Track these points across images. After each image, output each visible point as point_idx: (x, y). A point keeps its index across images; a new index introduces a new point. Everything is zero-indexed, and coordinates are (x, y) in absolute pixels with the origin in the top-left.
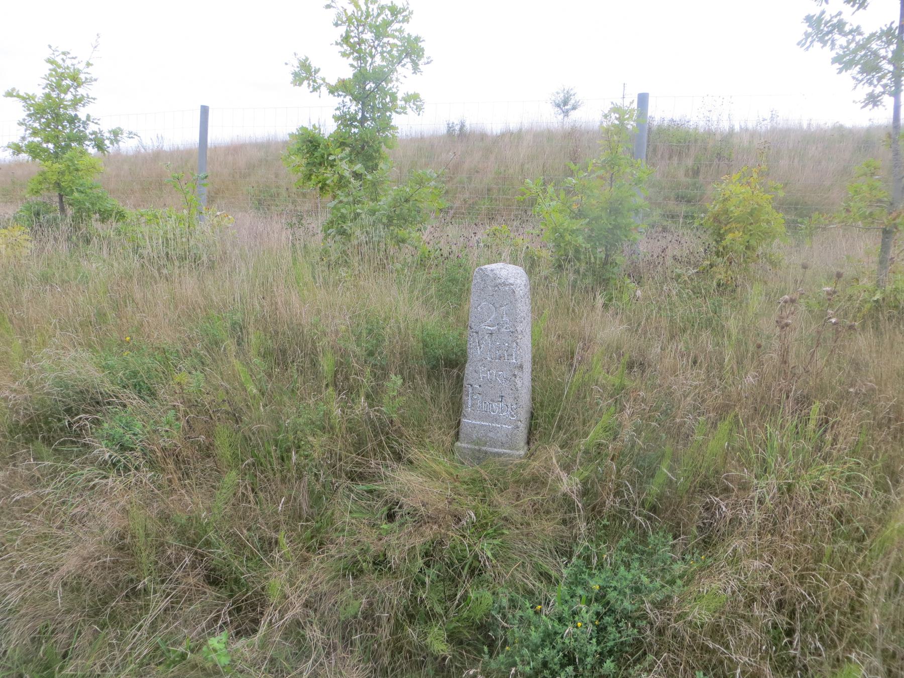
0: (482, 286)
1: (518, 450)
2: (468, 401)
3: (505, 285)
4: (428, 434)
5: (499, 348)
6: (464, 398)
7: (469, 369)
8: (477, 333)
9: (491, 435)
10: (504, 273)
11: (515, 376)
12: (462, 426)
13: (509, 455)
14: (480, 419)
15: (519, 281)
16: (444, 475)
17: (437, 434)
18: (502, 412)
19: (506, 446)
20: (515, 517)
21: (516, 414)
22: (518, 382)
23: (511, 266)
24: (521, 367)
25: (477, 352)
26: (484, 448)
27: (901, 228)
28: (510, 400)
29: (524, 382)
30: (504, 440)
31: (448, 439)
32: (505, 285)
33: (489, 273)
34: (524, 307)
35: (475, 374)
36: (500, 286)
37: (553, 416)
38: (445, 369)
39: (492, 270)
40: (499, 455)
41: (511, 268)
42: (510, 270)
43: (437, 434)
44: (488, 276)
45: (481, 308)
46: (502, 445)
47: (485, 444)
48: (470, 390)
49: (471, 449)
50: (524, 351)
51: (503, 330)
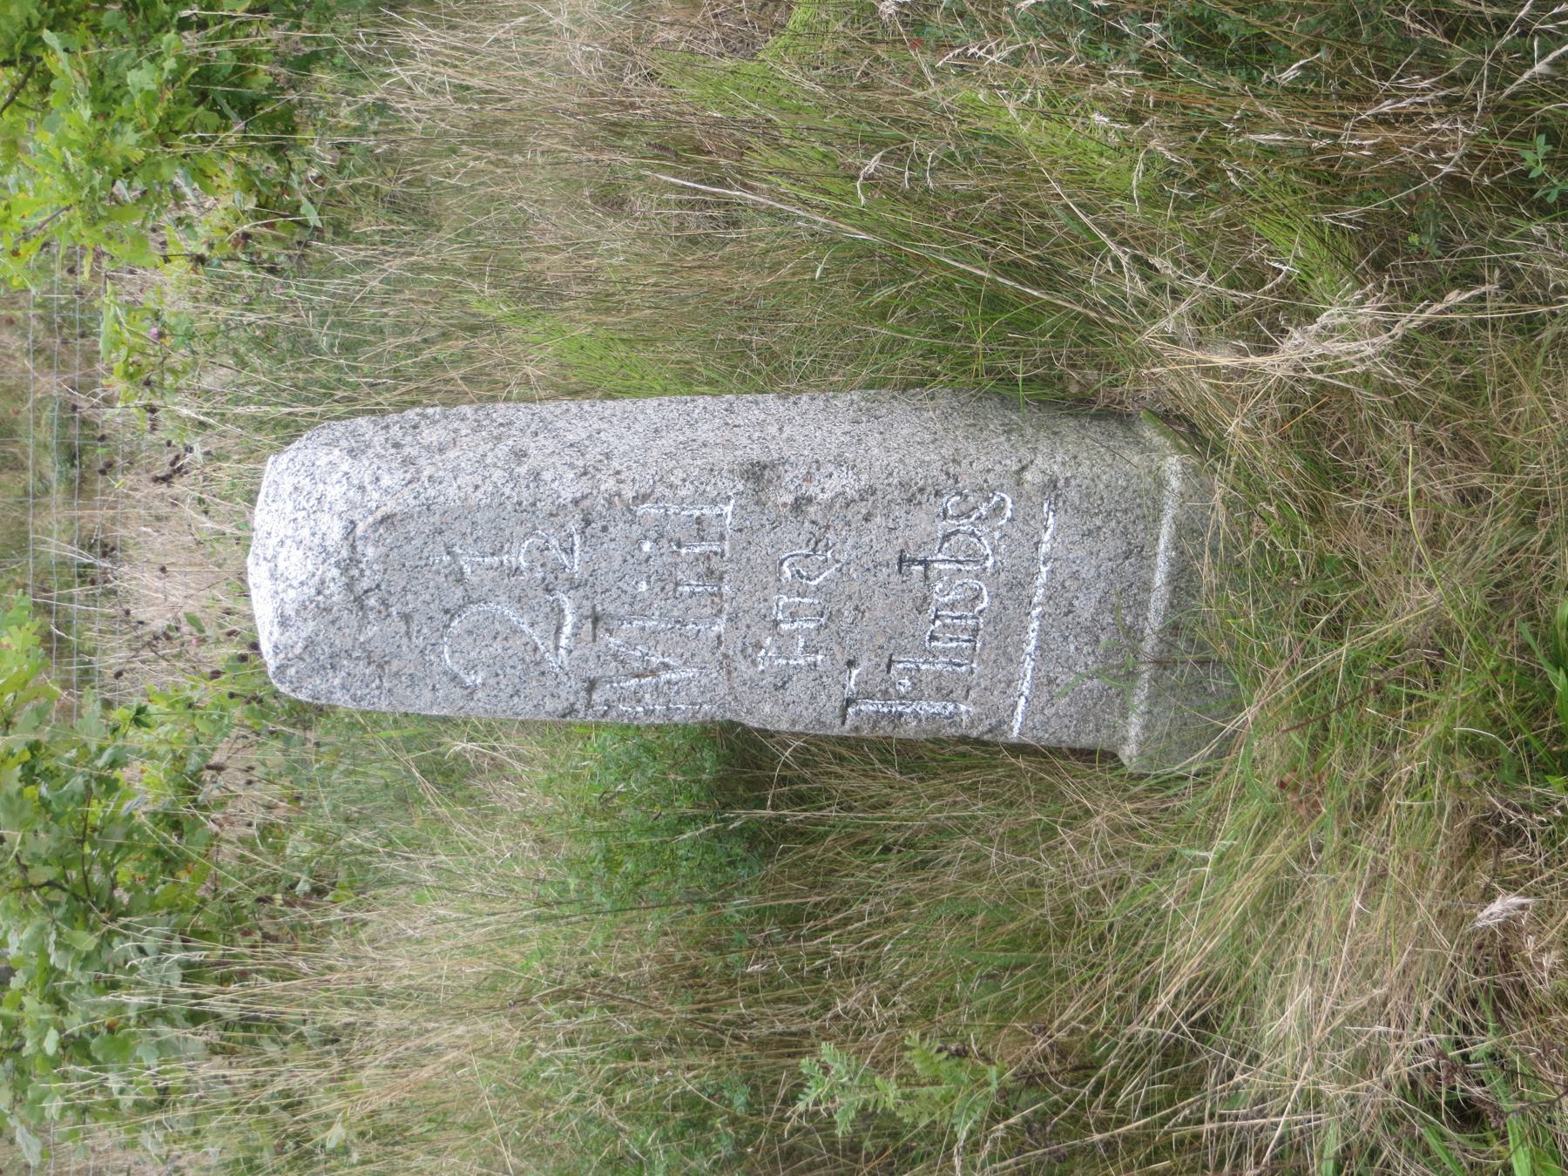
0: (361, 669)
1: (1161, 483)
2: (924, 713)
3: (353, 561)
4: (1082, 911)
5: (667, 582)
6: (909, 730)
7: (765, 714)
8: (592, 686)
9: (1086, 608)
10: (296, 564)
11: (799, 505)
12: (1046, 738)
13: (1187, 530)
14: (1008, 656)
15: (334, 492)
16: (1278, 851)
17: (1078, 864)
18: (976, 558)
19: (1139, 535)
20: (1489, 550)
21: (985, 491)
22: (833, 486)
23: (262, 517)
24: (757, 474)
25: (685, 682)
26: (1149, 645)
27: (1092, 1172)
28: (923, 525)
29: (825, 437)
30: (1114, 545)
31: (1106, 812)
32: (353, 561)
33: (296, 638)
34: (461, 456)
35: (796, 688)
36: (373, 580)
37: (996, 302)
38: (762, 816)
39: (284, 622)
40: (1183, 577)
41: (267, 518)
42: (283, 529)
43: (1078, 864)
44: (310, 644)
45: (471, 667)
46: (1138, 553)
47: (1133, 634)
48: (868, 707)
49: (1154, 698)
50: (665, 444)
51: (576, 565)
